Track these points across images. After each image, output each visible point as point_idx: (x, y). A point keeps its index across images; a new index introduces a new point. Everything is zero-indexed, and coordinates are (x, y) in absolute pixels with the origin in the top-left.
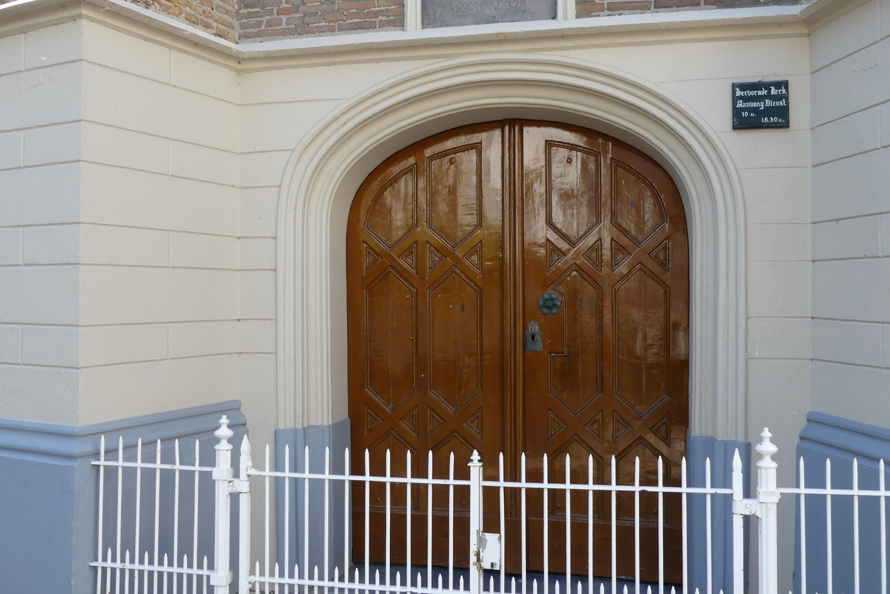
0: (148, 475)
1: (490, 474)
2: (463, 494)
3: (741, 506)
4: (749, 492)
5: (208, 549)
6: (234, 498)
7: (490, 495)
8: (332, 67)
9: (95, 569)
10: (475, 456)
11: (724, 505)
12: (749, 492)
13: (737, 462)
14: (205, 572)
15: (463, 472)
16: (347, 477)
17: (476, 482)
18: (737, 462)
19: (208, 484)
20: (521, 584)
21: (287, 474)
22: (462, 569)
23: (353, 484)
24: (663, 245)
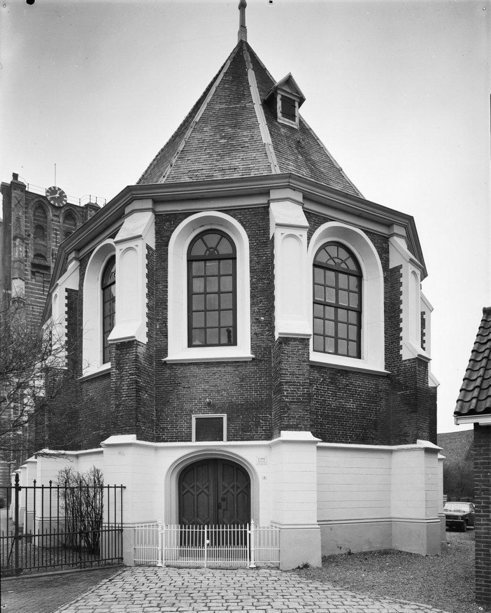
0: (215, 532)
1: (208, 528)
2: (204, 532)
3: (248, 532)
4: (250, 530)
5: (157, 543)
6: (162, 534)
7: (208, 532)
8: (144, 201)
9: (135, 548)
10: (206, 526)
11: (246, 532)
12: (250, 530)
13: (248, 525)
14: (157, 547)
15: (204, 529)
16: (214, 530)
17: (206, 530)
18: (248, 525)
19: (157, 531)
20: (255, 321)
21: (217, 530)
22: (203, 545)
23: (224, 529)
24: (149, 605)
